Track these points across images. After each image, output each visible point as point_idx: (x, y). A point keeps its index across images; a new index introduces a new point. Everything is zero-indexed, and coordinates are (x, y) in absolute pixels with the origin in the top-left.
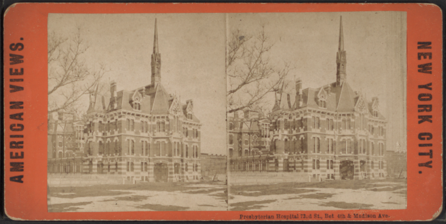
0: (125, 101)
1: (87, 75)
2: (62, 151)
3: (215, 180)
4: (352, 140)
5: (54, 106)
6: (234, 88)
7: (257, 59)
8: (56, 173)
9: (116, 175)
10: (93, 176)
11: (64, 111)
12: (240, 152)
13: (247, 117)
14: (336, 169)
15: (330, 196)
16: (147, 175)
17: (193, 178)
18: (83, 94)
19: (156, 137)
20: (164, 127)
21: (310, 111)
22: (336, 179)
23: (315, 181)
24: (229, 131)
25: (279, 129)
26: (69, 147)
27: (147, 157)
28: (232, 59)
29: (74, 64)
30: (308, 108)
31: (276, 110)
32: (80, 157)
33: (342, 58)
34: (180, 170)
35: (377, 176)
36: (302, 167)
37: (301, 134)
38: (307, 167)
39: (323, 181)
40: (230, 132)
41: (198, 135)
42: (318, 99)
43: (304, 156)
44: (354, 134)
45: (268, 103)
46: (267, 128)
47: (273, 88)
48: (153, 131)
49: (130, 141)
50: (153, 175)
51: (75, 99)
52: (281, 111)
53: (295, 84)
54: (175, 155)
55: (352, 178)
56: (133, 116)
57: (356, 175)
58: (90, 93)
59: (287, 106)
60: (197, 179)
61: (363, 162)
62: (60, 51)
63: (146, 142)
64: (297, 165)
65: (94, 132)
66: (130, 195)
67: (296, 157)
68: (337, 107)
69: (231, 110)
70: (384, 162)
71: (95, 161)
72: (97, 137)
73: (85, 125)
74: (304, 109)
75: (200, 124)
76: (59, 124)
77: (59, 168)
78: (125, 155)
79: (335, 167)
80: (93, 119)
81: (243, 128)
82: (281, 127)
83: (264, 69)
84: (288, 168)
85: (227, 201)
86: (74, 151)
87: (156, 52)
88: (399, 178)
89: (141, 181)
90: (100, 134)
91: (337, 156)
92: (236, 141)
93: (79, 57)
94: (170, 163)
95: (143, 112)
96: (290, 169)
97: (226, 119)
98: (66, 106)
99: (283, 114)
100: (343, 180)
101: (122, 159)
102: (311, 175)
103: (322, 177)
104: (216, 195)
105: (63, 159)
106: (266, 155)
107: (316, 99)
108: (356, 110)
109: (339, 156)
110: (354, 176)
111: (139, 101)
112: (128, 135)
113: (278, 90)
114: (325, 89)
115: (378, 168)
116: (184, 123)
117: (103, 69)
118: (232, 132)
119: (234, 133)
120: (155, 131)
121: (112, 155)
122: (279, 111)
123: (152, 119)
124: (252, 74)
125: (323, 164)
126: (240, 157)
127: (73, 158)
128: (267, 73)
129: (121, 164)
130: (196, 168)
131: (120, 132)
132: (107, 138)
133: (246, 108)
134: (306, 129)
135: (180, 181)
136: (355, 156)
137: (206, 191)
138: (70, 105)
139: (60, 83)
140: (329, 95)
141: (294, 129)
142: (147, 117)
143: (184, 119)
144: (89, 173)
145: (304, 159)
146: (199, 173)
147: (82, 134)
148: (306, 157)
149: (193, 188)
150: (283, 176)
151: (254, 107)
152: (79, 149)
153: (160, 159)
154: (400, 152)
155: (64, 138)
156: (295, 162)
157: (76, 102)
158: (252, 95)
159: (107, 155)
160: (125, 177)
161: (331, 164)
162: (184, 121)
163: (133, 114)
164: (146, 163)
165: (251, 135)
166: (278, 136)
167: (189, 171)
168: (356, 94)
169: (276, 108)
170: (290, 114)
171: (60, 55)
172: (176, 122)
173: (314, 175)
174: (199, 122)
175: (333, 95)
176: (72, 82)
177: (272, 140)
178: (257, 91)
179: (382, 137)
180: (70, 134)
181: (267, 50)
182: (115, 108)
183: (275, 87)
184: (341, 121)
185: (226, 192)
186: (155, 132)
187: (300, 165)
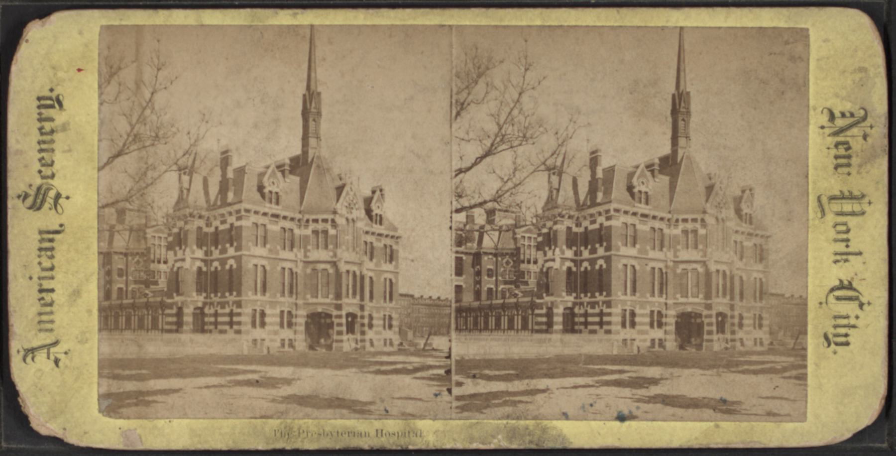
0: (619, 190)
1: (542, 133)
2: (122, 286)
3: (427, 348)
5: (477, 196)
6: (465, 165)
7: (512, 105)
8: (492, 330)
9: (601, 334)
10: (555, 337)
11: (128, 205)
12: (478, 294)
13: (490, 221)
14: (668, 328)
15: (654, 382)
16: (292, 336)
17: (382, 342)
18: (166, 171)
19: (311, 259)
20: (326, 241)
21: (247, 211)
23: (625, 352)
24: (455, 249)
27: (662, 300)
28: (462, 104)
29: (515, 112)
30: (244, 205)
31: (548, 210)
32: (159, 299)
33: (313, 105)
34: (357, 327)
35: (749, 343)
36: (231, 324)
38: (609, 323)
40: (457, 252)
42: (634, 187)
43: (604, 302)
44: (334, 259)
45: (533, 194)
46: (532, 244)
47: (544, 163)
48: (305, 248)
49: (629, 267)
50: (673, 336)
51: (518, 182)
53: (587, 158)
55: (699, 347)
57: (337, 341)
58: (180, 170)
59: (202, 202)
60: (762, 344)
61: (352, 316)
62: (120, 85)
63: (291, 270)
64: (220, 319)
65: (557, 250)
66: (624, 376)
68: (671, 204)
69: (459, 207)
70: (394, 316)
71: (557, 307)
72: (564, 259)
73: (169, 235)
74: (606, 207)
75: (768, 234)
76: (118, 231)
77: (117, 322)
78: (618, 294)
79: (666, 324)
80: (186, 223)
82: (559, 243)
84: (570, 326)
85: (450, 391)
86: (517, 287)
87: (313, 87)
88: (424, 349)
90: (569, 254)
91: (670, 302)
92: (469, 270)
93: (525, 98)
94: (339, 313)
95: (656, 208)
96: (206, 327)
97: (449, 224)
98: (500, 197)
99: (563, 217)
100: (311, 352)
101: (243, 303)
102: (248, 341)
103: (641, 344)
104: (430, 379)
105: (494, 302)
107: (630, 188)
108: (339, 212)
109: (675, 304)
110: (704, 344)
111: (647, 187)
112: (255, 255)
113: (554, 168)
114: (278, 167)
115: (751, 328)
116: (737, 232)
118: (462, 253)
119: (466, 254)
120: (679, 247)
121: (223, 296)
122: (556, 211)
123: (303, 223)
124: (135, 136)
126: (478, 303)
127: (145, 300)
129: (609, 314)
130: (388, 323)
131: (238, 249)
132: (212, 261)
133: (490, 205)
134: (608, 249)
135: (726, 349)
138: (508, 193)
139: (486, 149)
141: (232, 245)
142: (662, 219)
143: (366, 225)
144: (177, 331)
147: (533, 253)
148: (609, 304)
149: (382, 363)
151: (506, 200)
152: (526, 283)
153: (316, 304)
154: (797, 296)
155: (497, 260)
156: (586, 315)
157: (520, 188)
158: (502, 179)
159: (597, 294)
160: (617, 341)
161: (657, 320)
162: (367, 229)
163: (265, 214)
164: (289, 312)
165: (500, 259)
166: (553, 260)
167: (374, 329)
168: (710, 179)
169: (182, 206)
170: (578, 218)
171: (119, 92)
172: (351, 230)
173: (625, 340)
174: (395, 229)
175: (295, 180)
176: (512, 147)
177: (172, 269)
178: (512, 171)
179: (760, 267)
180: (509, 252)
181: (533, 88)
182: (599, 200)
183: (548, 163)
184: (308, 232)
185: (448, 372)
186: (309, 251)
187: (227, 319)
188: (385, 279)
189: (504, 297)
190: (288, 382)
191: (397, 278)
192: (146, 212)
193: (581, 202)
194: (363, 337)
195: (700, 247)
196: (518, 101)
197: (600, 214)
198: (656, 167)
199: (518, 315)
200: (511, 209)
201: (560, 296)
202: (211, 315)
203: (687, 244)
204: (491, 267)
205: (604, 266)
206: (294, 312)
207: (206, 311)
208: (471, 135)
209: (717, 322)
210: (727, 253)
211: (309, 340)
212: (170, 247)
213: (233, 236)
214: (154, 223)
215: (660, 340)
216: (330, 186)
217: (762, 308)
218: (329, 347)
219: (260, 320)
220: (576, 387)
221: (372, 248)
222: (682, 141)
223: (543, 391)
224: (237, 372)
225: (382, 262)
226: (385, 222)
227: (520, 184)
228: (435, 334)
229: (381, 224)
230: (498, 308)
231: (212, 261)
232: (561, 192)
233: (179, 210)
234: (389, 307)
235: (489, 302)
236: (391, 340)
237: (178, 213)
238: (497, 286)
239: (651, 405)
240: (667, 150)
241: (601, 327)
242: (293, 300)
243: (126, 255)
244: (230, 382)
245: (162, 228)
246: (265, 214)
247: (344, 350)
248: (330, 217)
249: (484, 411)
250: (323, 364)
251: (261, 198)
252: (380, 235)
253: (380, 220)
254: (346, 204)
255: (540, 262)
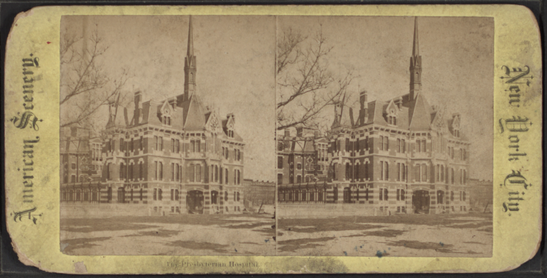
0: (378, 116)
1: (331, 81)
2: (301, 175)
3: (261, 212)
4: (428, 164)
5: (291, 119)
6: (284, 101)
7: (313, 64)
8: (300, 201)
9: (367, 204)
10: (339, 205)
11: (78, 125)
12: (292, 180)
13: (299, 135)
14: (408, 200)
15: (399, 233)
16: (178, 205)
17: (233, 209)
18: (101, 104)
19: (189, 158)
20: (425, 147)
21: (151, 128)
22: (181, 212)
23: (382, 214)
24: (278, 152)
25: (114, 150)
26: (310, 170)
27: (404, 183)
28: (282, 63)
30: (149, 125)
31: (335, 128)
32: (97, 182)
34: (218, 200)
35: (457, 209)
36: (141, 197)
37: (140, 157)
38: (372, 197)
39: (392, 214)
40: (279, 154)
41: (241, 156)
42: (387, 114)
44: (204, 158)
45: (326, 119)
46: (325, 149)
47: (332, 100)
48: (186, 151)
49: (384, 163)
51: (316, 111)
52: (342, 128)
53: (358, 96)
54: (438, 181)
55: (427, 211)
56: (387, 132)
58: (110, 103)
59: (123, 123)
60: (465, 210)
61: (215, 193)
62: (73, 52)
63: (178, 164)
64: (134, 195)
66: (381, 230)
67: (143, 184)
69: (280, 126)
70: (241, 192)
71: (340, 187)
72: (344, 158)
73: (103, 143)
74: (370, 126)
75: (469, 143)
76: (72, 141)
77: (71, 196)
78: (377, 179)
79: (406, 197)
80: (114, 136)
81: (70, 149)
82: (341, 148)
83: (321, 76)
84: (348, 199)
86: (316, 175)
87: (191, 53)
88: (259, 213)
89: (397, 212)
90: (122, 155)
91: (409, 184)
92: (286, 165)
93: (320, 60)
94: (207, 191)
95: (400, 127)
96: (126, 200)
98: (305, 120)
99: (344, 132)
100: (190, 215)
101: (148, 185)
102: (151, 208)
103: (391, 210)
104: (262, 231)
105: (302, 184)
106: (322, 182)
107: (385, 115)
108: (207, 129)
109: (412, 185)
110: (430, 210)
112: (156, 156)
113: (338, 103)
114: (170, 102)
116: (450, 141)
117: (126, 74)
118: (282, 154)
119: (285, 155)
120: (414, 151)
122: (340, 129)
123: (185, 136)
124: (83, 83)
125: (166, 194)
126: (292, 185)
127: (88, 183)
128: (101, 82)
129: (372, 192)
130: (463, 197)
131: (145, 152)
132: (129, 159)
133: (299, 125)
134: (371, 152)
135: (443, 212)
136: (430, 185)
137: (250, 226)
138: (310, 118)
139: (297, 91)
140: (401, 110)
141: (141, 149)
142: (404, 134)
143: (224, 137)
145: (143, 188)
146: (241, 203)
147: (325, 154)
148: (372, 185)
149: (233, 221)
150: (117, 208)
151: (309, 122)
152: (321, 173)
154: (486, 180)
155: (303, 159)
156: (358, 192)
158: (307, 109)
159: (364, 179)
160: (377, 208)
161: (401, 195)
162: (224, 139)
164: (177, 191)
165: (305, 158)
166: (338, 159)
167: (229, 200)
168: (434, 109)
169: (111, 125)
171: (73, 56)
172: (214, 141)
173: (381, 207)
174: (241, 140)
176: (312, 90)
177: (105, 164)
178: (312, 104)
179: (464, 163)
180: (311, 153)
182: (366, 122)
183: (335, 99)
184: (188, 141)
185: (274, 227)
186: (189, 153)
187: (139, 194)
188: (235, 170)
189: (307, 181)
190: (176, 233)
191: (242, 170)
192: (89, 129)
193: (355, 123)
194: (221, 206)
195: (428, 150)
196: (316, 61)
197: (366, 130)
198: (401, 102)
199: (316, 192)
200: (312, 128)
201: (342, 180)
202: (129, 192)
203: (420, 149)
204: (300, 163)
205: (369, 162)
206: (179, 190)
207: (126, 189)
208: (288, 82)
209: (438, 196)
210: (444, 154)
211: (189, 207)
212: (104, 151)
213: (142, 144)
214: (94, 136)
215: (403, 207)
216: (202, 113)
217: (465, 188)
218: (201, 212)
219: (158, 195)
220: (351, 236)
221: (227, 151)
222: (416, 86)
223: (332, 238)
224: (145, 227)
225: (233, 160)
226: (235, 135)
227: (93, 112)
228: (266, 204)
229: (232, 136)
230: (304, 188)
231: (129, 159)
232: (343, 117)
233: (109, 128)
234: (238, 187)
235: (298, 184)
236: (238, 207)
237: (109, 130)
238: (303, 174)
239: (397, 247)
240: (407, 91)
241: (367, 200)
242: (179, 183)
243: (77, 155)
244: (140, 233)
245: (99, 139)
246: (162, 131)
247: (210, 213)
248: (201, 132)
249: (296, 250)
250: (197, 222)
251: (159, 121)
252: (232, 143)
253: (232, 134)
254: (211, 124)
255: (330, 160)
